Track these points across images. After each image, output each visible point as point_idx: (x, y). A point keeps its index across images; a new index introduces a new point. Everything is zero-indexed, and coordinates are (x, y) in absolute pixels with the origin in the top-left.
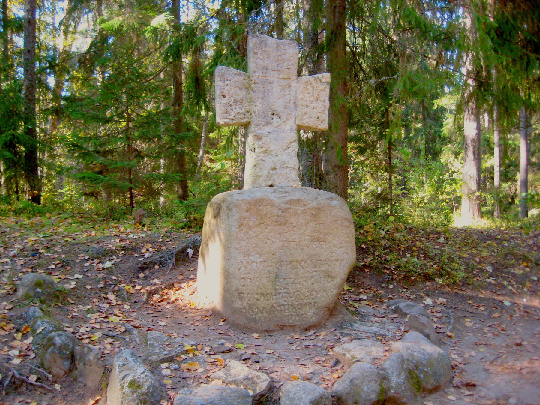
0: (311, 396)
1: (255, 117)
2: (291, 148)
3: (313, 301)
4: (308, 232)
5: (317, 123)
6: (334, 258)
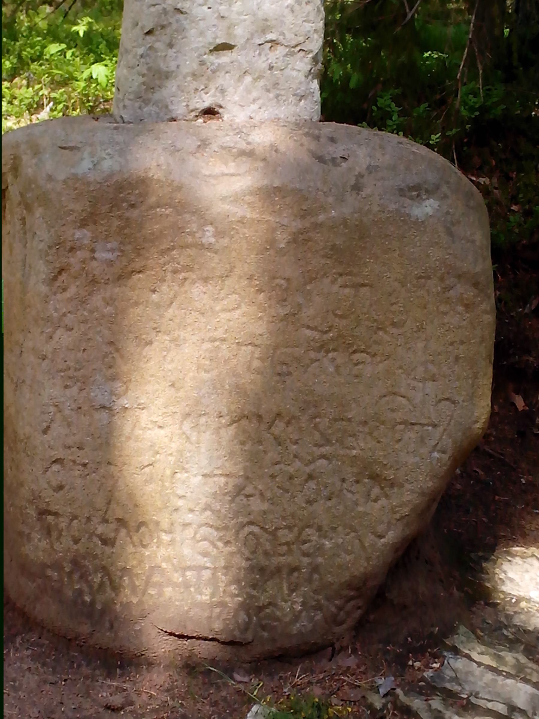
6: (398, 416)
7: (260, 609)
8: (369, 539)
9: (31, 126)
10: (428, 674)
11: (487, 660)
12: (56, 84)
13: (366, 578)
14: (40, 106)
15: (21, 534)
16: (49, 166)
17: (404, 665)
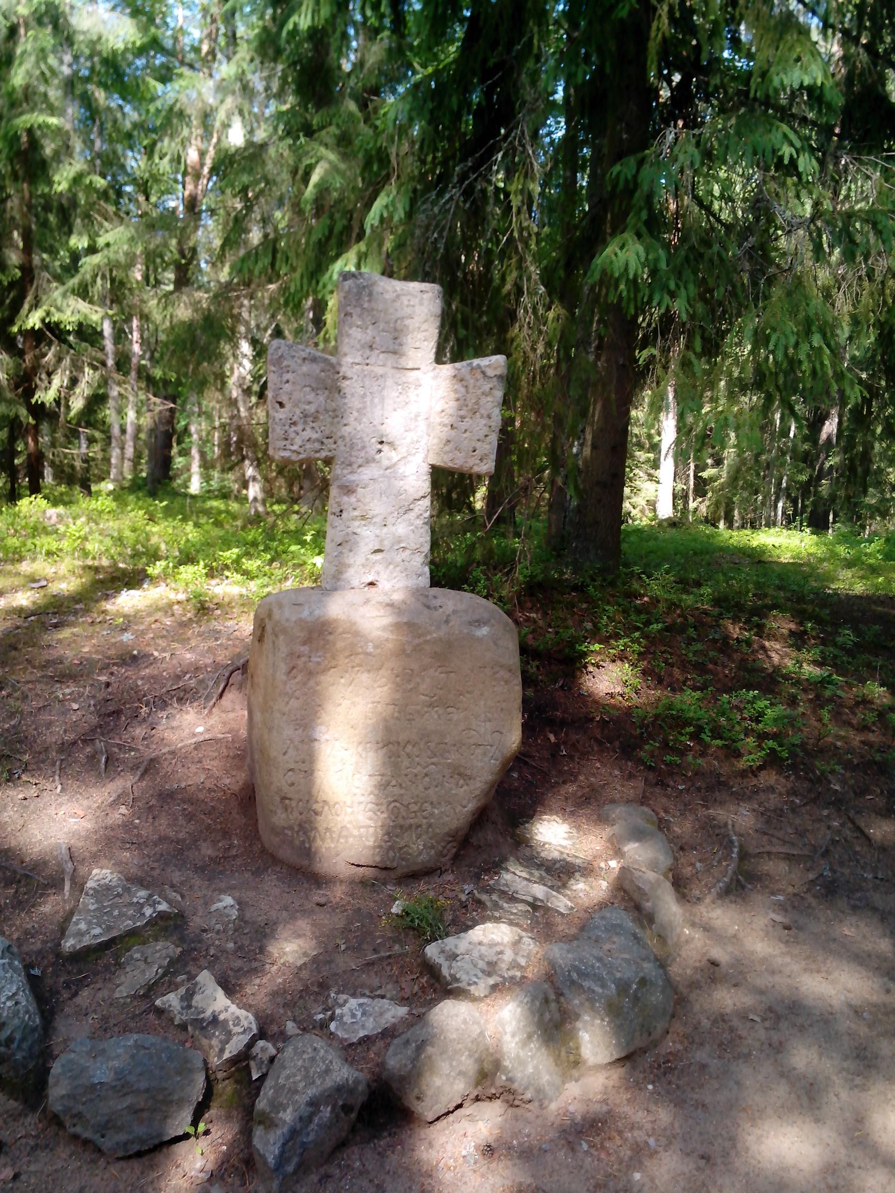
0: (314, 1090)
1: (342, 448)
2: (416, 510)
3: (425, 821)
4: (423, 687)
5: (471, 462)
6: (472, 741)
7: (401, 849)
8: (459, 808)
9: (281, 592)
10: (492, 882)
11: (524, 875)
12: (296, 566)
13: (457, 830)
14: (286, 579)
15: (271, 811)
16: (287, 613)
17: (479, 878)
